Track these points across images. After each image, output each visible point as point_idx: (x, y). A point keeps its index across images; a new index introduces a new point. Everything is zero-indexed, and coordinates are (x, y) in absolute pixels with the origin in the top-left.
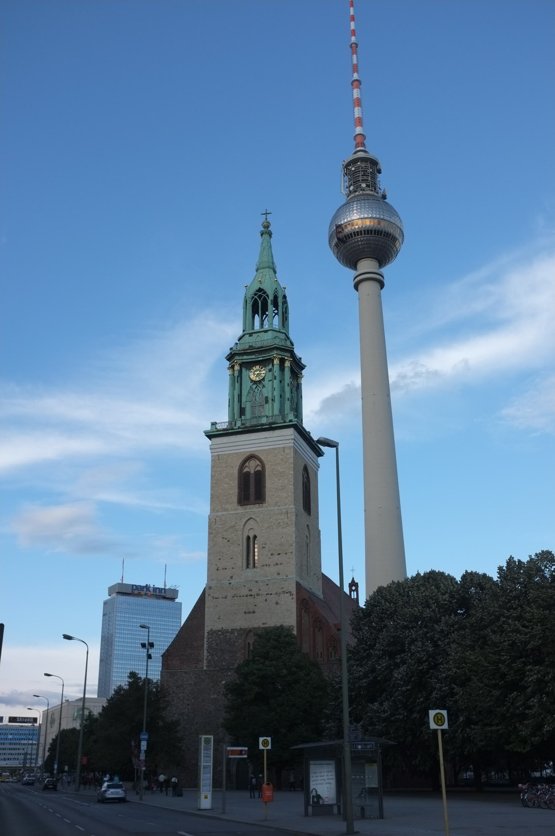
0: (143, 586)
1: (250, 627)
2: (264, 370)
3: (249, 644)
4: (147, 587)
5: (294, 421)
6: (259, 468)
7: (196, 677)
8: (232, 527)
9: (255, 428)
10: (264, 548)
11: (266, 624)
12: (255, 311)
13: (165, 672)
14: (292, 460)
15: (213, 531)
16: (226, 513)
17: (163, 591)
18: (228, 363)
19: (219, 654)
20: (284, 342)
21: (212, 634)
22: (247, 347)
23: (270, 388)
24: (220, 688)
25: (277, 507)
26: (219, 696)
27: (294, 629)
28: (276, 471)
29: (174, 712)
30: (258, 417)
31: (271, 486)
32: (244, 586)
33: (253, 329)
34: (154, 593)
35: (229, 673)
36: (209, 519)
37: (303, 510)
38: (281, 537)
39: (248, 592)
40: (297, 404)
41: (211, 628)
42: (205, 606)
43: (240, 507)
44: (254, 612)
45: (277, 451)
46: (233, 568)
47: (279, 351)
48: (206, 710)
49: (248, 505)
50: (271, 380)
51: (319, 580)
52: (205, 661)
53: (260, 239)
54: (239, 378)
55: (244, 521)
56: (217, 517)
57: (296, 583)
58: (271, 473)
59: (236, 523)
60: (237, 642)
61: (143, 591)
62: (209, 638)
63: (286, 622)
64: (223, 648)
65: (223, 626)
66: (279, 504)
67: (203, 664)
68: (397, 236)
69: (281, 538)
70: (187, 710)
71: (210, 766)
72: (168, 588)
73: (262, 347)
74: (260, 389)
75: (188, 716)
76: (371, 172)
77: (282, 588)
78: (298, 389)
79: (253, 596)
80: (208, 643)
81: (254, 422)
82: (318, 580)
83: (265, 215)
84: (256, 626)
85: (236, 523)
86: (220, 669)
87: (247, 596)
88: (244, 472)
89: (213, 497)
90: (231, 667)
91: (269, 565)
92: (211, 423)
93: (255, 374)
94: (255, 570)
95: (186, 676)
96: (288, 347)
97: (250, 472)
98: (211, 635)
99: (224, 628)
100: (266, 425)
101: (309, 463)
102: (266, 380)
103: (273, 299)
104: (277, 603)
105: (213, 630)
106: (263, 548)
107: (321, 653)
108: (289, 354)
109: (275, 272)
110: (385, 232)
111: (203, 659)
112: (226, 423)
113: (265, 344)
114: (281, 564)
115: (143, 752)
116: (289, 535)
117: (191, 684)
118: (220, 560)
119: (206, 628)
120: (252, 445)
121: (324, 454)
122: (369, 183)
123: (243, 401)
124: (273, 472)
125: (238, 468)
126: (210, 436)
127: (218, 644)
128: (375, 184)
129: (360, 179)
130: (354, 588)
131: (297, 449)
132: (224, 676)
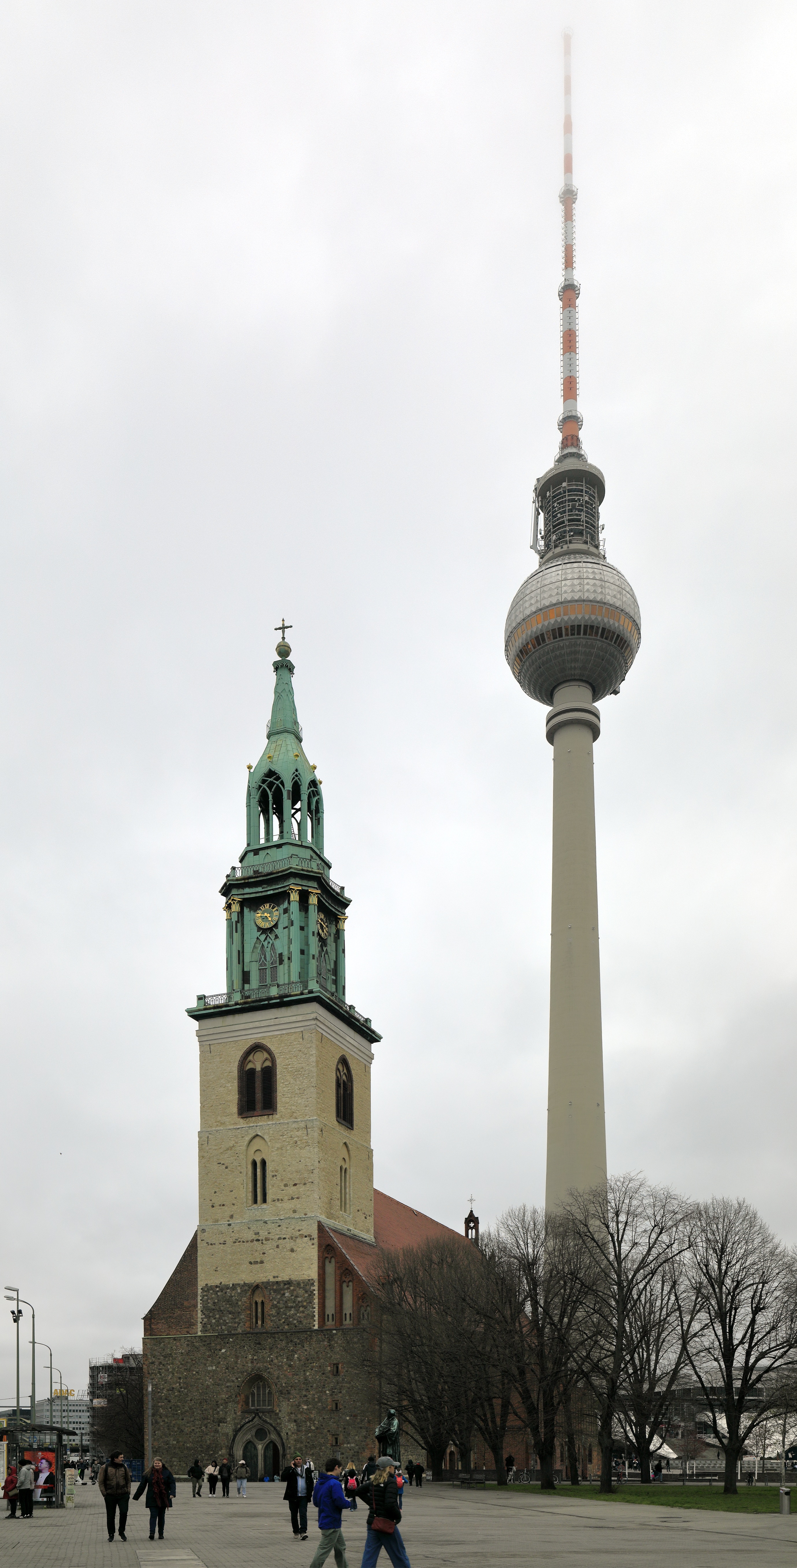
2: (277, 910)
3: (256, 1303)
5: (317, 992)
6: (268, 1064)
7: (188, 1345)
8: (231, 1148)
9: (259, 1003)
10: (275, 1177)
11: (277, 1277)
12: (263, 803)
13: (148, 1338)
15: (206, 1154)
18: (224, 899)
20: (306, 862)
22: (251, 873)
24: (220, 1358)
26: (218, 1367)
27: (315, 1284)
29: (162, 1387)
30: (269, 985)
32: (249, 1228)
35: (231, 1340)
37: (336, 1123)
38: (298, 1161)
39: (254, 1236)
40: (336, 963)
43: (241, 1120)
44: (262, 1262)
45: (293, 1037)
46: (233, 1204)
47: (297, 879)
50: (286, 927)
51: (368, 1218)
52: (199, 1325)
53: (272, 677)
54: (239, 925)
55: (248, 1138)
58: (285, 1070)
59: (236, 1143)
60: (241, 1300)
62: (204, 1296)
64: (222, 1308)
65: (222, 1280)
66: (295, 1114)
67: (197, 1328)
70: (178, 1384)
73: (272, 874)
74: (271, 942)
75: (179, 1392)
77: (299, 1231)
78: (339, 938)
79: (260, 1242)
80: (203, 1301)
81: (263, 995)
82: (366, 1218)
83: (281, 630)
84: (265, 1280)
85: (236, 1143)
87: (252, 1241)
89: (204, 1106)
90: (233, 1332)
93: (265, 916)
94: (264, 1206)
96: (312, 872)
97: (255, 1069)
98: (206, 1291)
99: (223, 1283)
100: (275, 998)
101: (352, 1053)
102: (280, 926)
103: (291, 789)
104: (292, 1250)
105: (209, 1285)
106: (273, 1176)
108: (316, 883)
109: (300, 740)
112: (224, 996)
114: (298, 1198)
117: (182, 1353)
118: (217, 1194)
120: (219, 1035)
121: (381, 1038)
122: (583, 525)
125: (237, 1064)
126: (196, 1015)
128: (594, 527)
130: (472, 1225)
131: (324, 1033)
132: (224, 1343)
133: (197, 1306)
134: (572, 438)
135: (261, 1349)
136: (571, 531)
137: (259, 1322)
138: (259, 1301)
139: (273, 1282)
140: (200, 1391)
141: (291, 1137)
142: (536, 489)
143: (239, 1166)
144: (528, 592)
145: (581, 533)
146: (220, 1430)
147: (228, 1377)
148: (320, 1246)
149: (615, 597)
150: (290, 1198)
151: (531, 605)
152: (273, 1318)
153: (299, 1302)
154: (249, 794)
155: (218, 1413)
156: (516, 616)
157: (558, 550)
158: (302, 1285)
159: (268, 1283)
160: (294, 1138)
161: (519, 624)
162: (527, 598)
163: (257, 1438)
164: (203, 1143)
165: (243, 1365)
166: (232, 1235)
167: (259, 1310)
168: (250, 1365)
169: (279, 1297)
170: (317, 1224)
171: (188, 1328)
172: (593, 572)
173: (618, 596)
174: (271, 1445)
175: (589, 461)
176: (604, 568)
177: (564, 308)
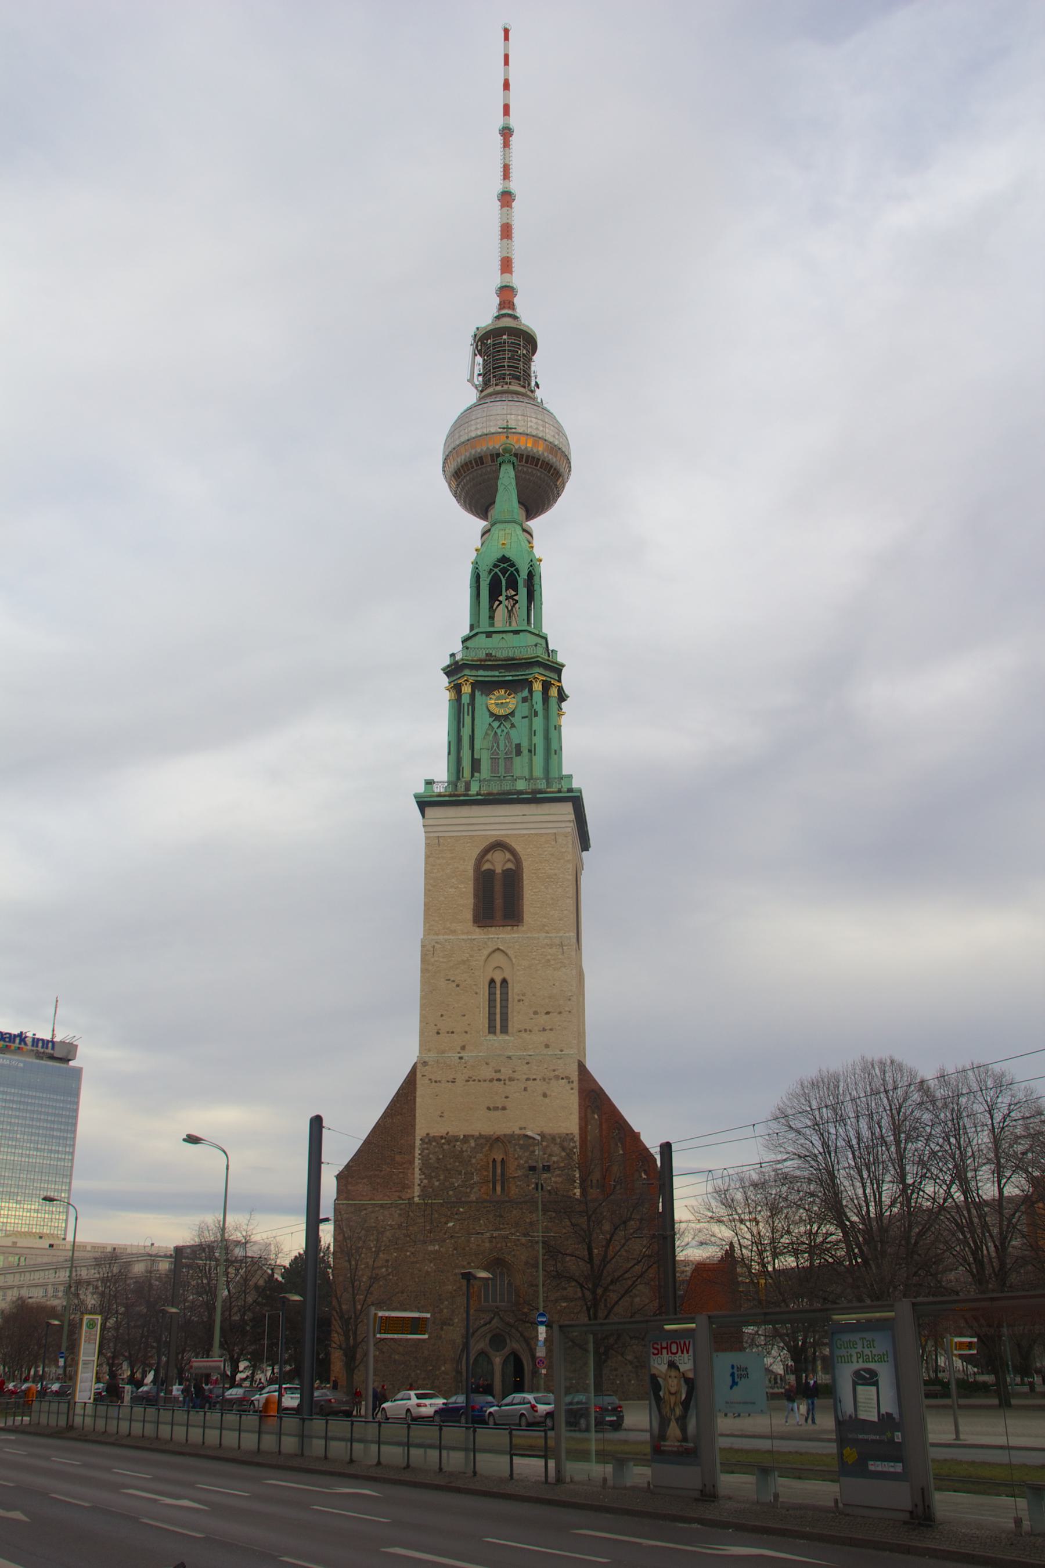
0: (15, 1035)
1: (497, 1134)
2: (514, 697)
4: (22, 1037)
6: (510, 866)
7: (400, 1215)
8: (464, 962)
9: (507, 797)
10: (521, 1002)
11: (525, 1128)
13: (343, 1204)
14: (569, 857)
15: (430, 968)
16: (453, 938)
17: (50, 1045)
19: (442, 1177)
21: (430, 1142)
22: (482, 656)
23: (525, 731)
25: (544, 935)
26: (442, 1247)
28: (542, 873)
31: (533, 897)
32: (487, 1064)
33: (492, 625)
34: (33, 1048)
35: (461, 1210)
36: (423, 946)
39: (494, 1074)
41: (426, 1132)
42: (415, 1093)
43: (477, 930)
44: (504, 1108)
46: (466, 1032)
48: (420, 1271)
49: (491, 926)
54: (470, 707)
55: (486, 952)
56: (436, 943)
57: (579, 1064)
60: (475, 1157)
61: (14, 1042)
62: (424, 1149)
63: (560, 1126)
65: (449, 1130)
66: (546, 928)
67: (414, 1192)
68: (562, 470)
69: (550, 986)
71: (94, 1361)
72: (59, 1040)
73: (513, 659)
74: (506, 731)
76: (523, 354)
77: (554, 1071)
79: (502, 1082)
81: (495, 788)
84: (508, 1132)
85: (471, 956)
86: (444, 1202)
87: (491, 1080)
88: (483, 869)
89: (428, 909)
90: (463, 1199)
91: (530, 1031)
92: (425, 780)
95: (383, 1213)
97: (494, 871)
98: (427, 1143)
102: (518, 716)
107: (653, 1184)
110: (543, 461)
111: (414, 1185)
113: (516, 654)
114: (551, 1030)
115: (541, 1344)
116: (565, 982)
118: (443, 1018)
119: (418, 1132)
122: (520, 373)
123: (475, 747)
124: (536, 873)
126: (424, 804)
127: (439, 1159)
129: (506, 364)
133: (414, 1163)
134: (509, 303)
135: (503, 1224)
136: (510, 374)
137: (499, 1188)
138: (499, 1159)
139: (519, 1135)
140: (417, 1280)
141: (541, 955)
142: (475, 335)
143: (475, 985)
144: (473, 418)
145: (518, 378)
146: (443, 1336)
147: (457, 1261)
148: (581, 1091)
149: (554, 436)
150: (541, 1029)
151: (477, 429)
152: (519, 1183)
153: (554, 1162)
154: (477, 578)
155: (441, 1312)
156: (460, 437)
157: (499, 388)
158: (558, 1140)
159: (512, 1135)
160: (546, 955)
161: (463, 443)
162: (472, 422)
163: (491, 1347)
164: (428, 953)
165: (477, 1245)
166: (465, 1071)
167: (499, 1171)
168: (487, 1245)
169: (526, 1154)
170: (577, 1064)
171: (401, 1191)
172: (535, 413)
173: (557, 437)
174: (512, 1358)
175: (523, 322)
176: (545, 411)
177: (502, 207)
